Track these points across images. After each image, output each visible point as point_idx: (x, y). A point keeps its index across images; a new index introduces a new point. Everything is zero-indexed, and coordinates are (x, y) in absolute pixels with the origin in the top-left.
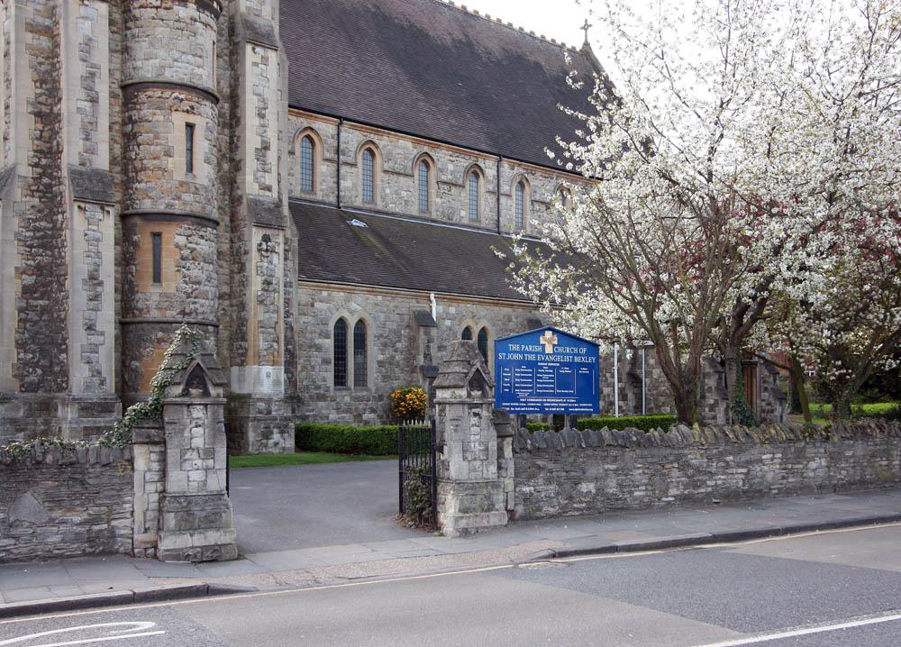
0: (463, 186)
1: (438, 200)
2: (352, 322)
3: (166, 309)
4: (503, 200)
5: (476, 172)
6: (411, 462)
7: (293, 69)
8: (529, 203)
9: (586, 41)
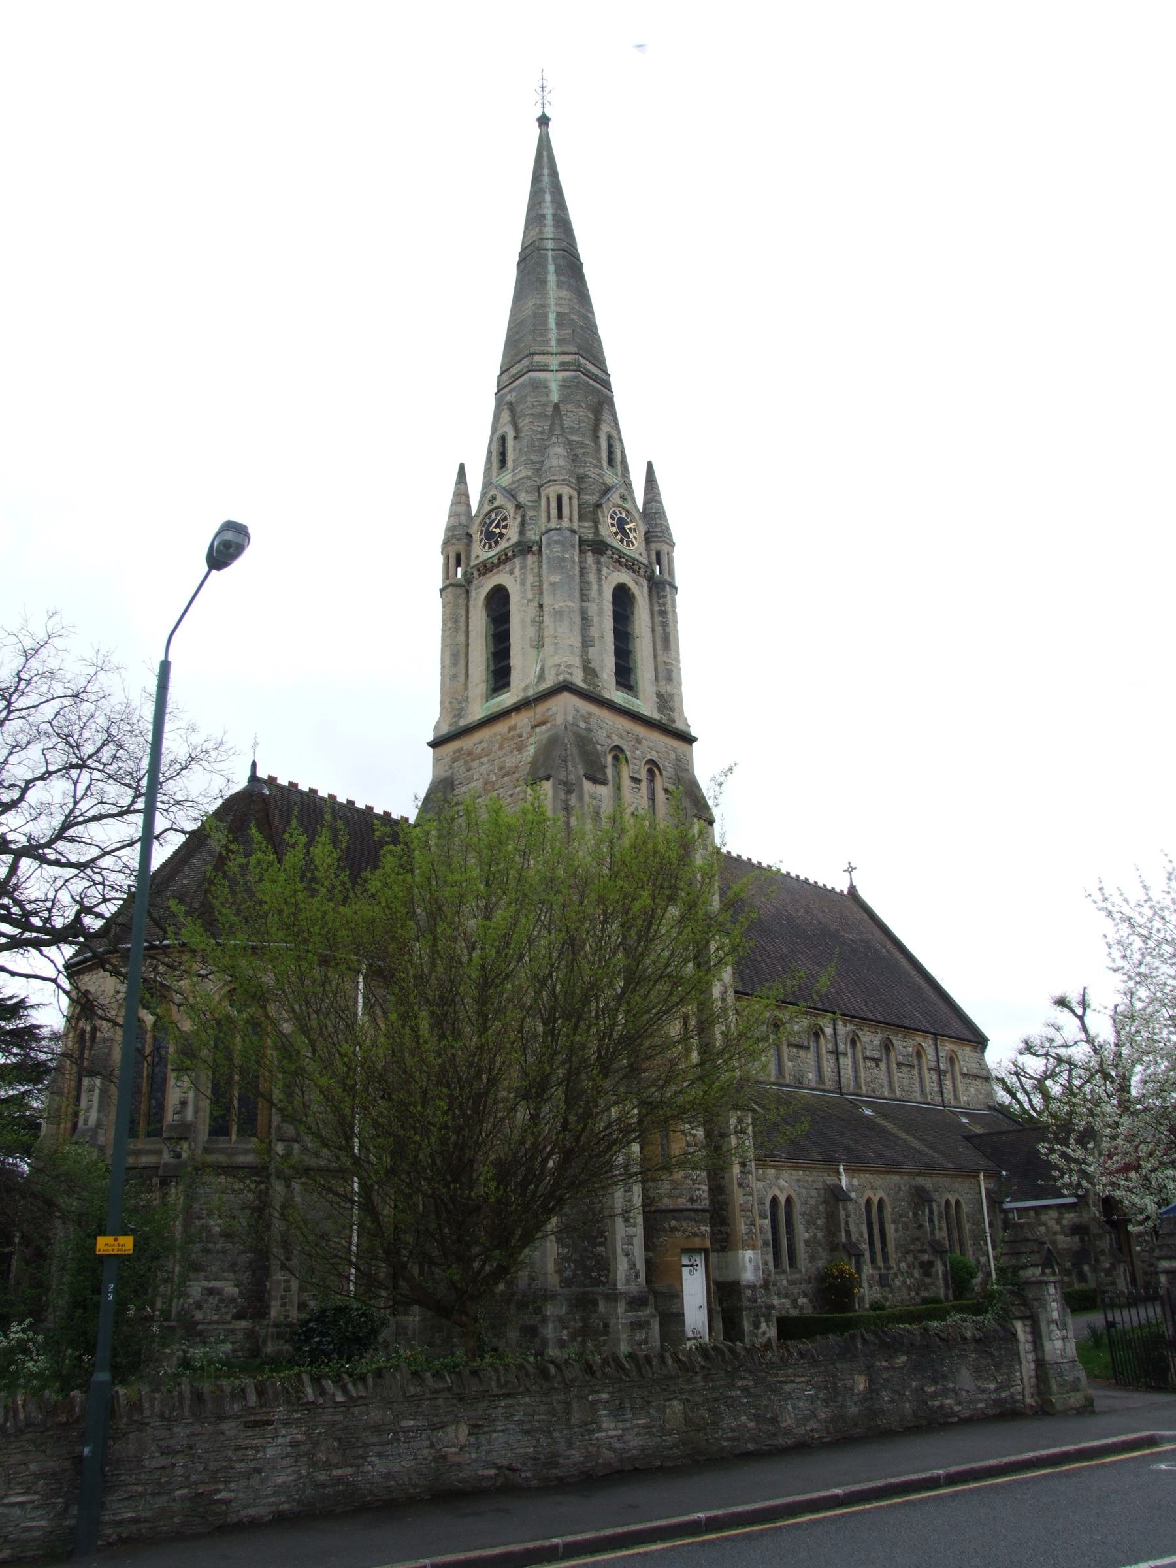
0: (808, 1048)
1: (790, 1064)
2: (782, 1199)
3: (677, 1197)
4: (842, 1060)
5: (817, 1033)
6: (1135, 1318)
7: (219, 839)
8: (861, 1060)
9: (851, 884)
